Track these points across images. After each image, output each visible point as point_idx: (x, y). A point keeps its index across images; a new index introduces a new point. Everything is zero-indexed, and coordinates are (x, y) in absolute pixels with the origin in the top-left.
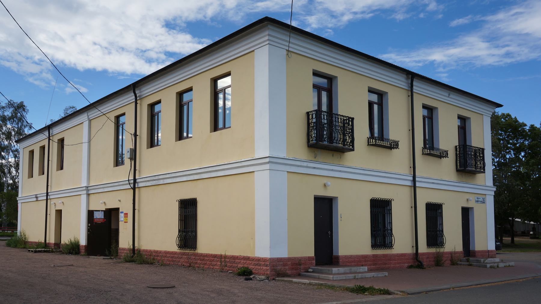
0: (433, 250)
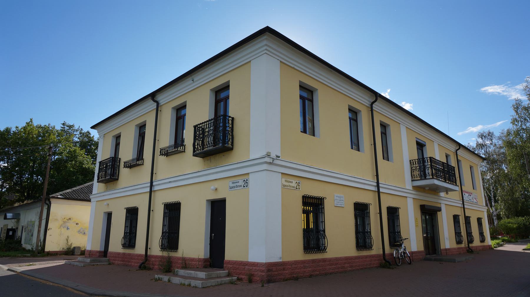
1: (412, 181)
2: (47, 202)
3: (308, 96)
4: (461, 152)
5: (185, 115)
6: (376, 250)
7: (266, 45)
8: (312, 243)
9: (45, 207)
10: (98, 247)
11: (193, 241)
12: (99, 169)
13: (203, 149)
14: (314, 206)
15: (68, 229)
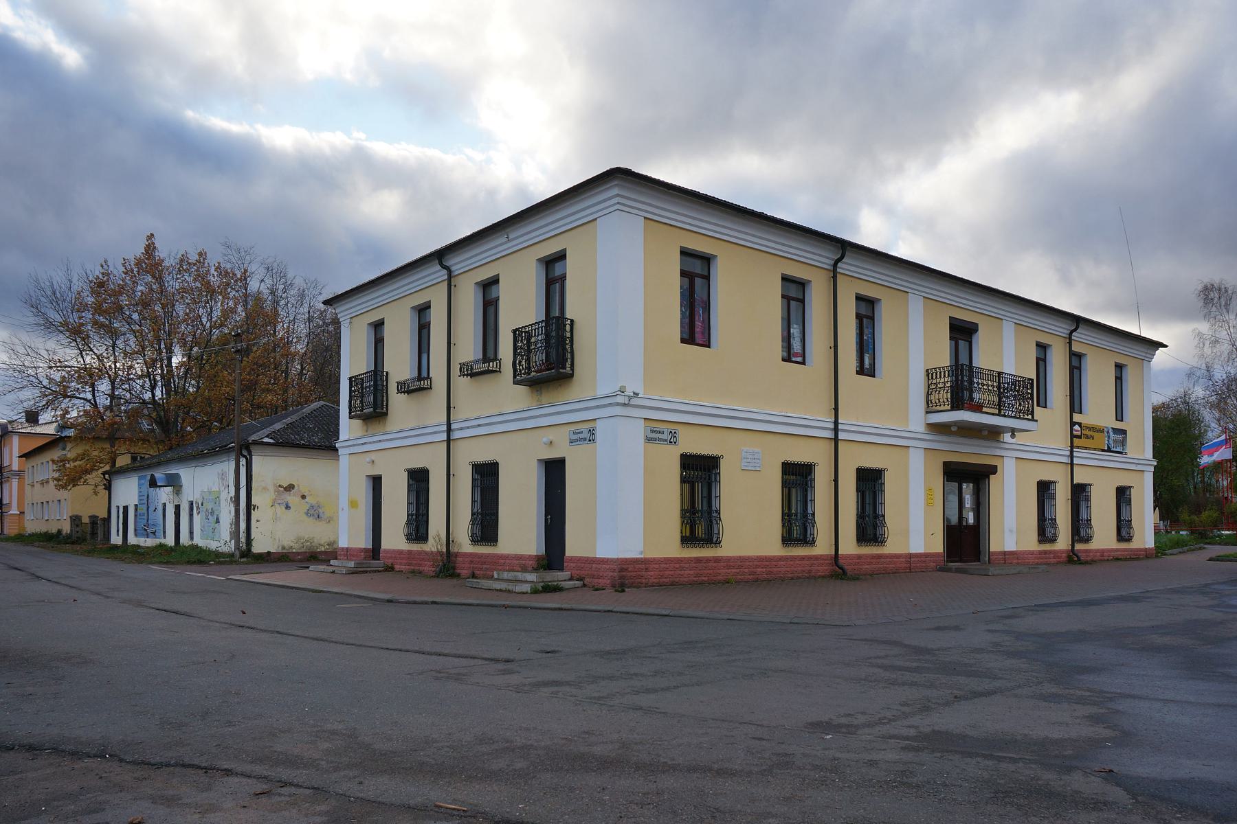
0: (415, 547)
2: (245, 453)
3: (696, 272)
4: (1081, 335)
5: (498, 299)
6: (823, 547)
7: (618, 195)
8: (700, 531)
9: (243, 461)
10: (363, 541)
11: (520, 532)
14: (700, 473)
15: (288, 507)
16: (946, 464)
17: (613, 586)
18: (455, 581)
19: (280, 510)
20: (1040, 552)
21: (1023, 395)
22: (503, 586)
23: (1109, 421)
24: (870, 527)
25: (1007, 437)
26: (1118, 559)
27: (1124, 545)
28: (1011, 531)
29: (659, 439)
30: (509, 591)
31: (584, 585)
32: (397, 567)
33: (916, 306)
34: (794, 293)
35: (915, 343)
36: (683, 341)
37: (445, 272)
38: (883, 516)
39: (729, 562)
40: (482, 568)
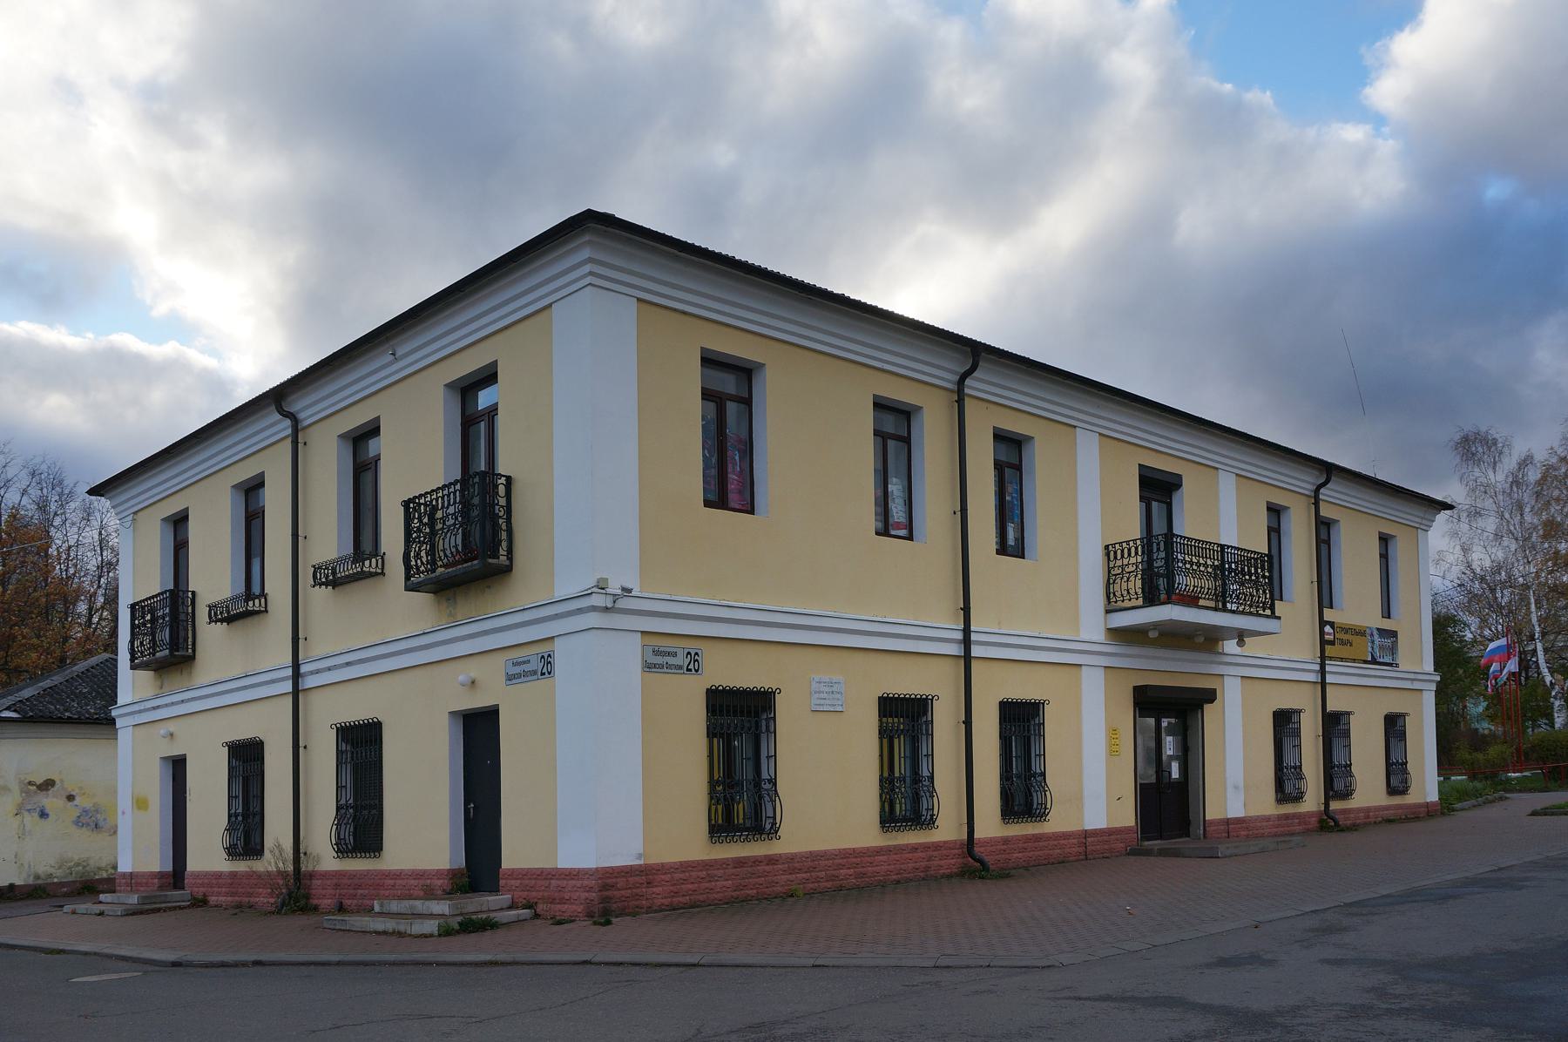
0: (241, 866)
1: (1108, 612)
3: (729, 392)
4: (1334, 493)
5: (377, 459)
6: (947, 828)
7: (590, 260)
8: (740, 811)
10: (156, 861)
11: (421, 826)
12: (133, 626)
13: (434, 571)
14: (740, 720)
15: (43, 815)
16: (1136, 689)
17: (590, 915)
18: (312, 919)
19: (30, 820)
20: (1280, 817)
21: (1252, 579)
22: (390, 925)
23: (1374, 620)
24: (1023, 793)
25: (1230, 646)
26: (1389, 821)
27: (1397, 800)
28: (1236, 787)
29: (669, 666)
30: (400, 934)
31: (537, 916)
32: (213, 900)
33: (1088, 449)
34: (894, 426)
35: (1086, 503)
36: (708, 504)
37: (288, 422)
38: (1043, 774)
39: (792, 862)
40: (353, 897)
